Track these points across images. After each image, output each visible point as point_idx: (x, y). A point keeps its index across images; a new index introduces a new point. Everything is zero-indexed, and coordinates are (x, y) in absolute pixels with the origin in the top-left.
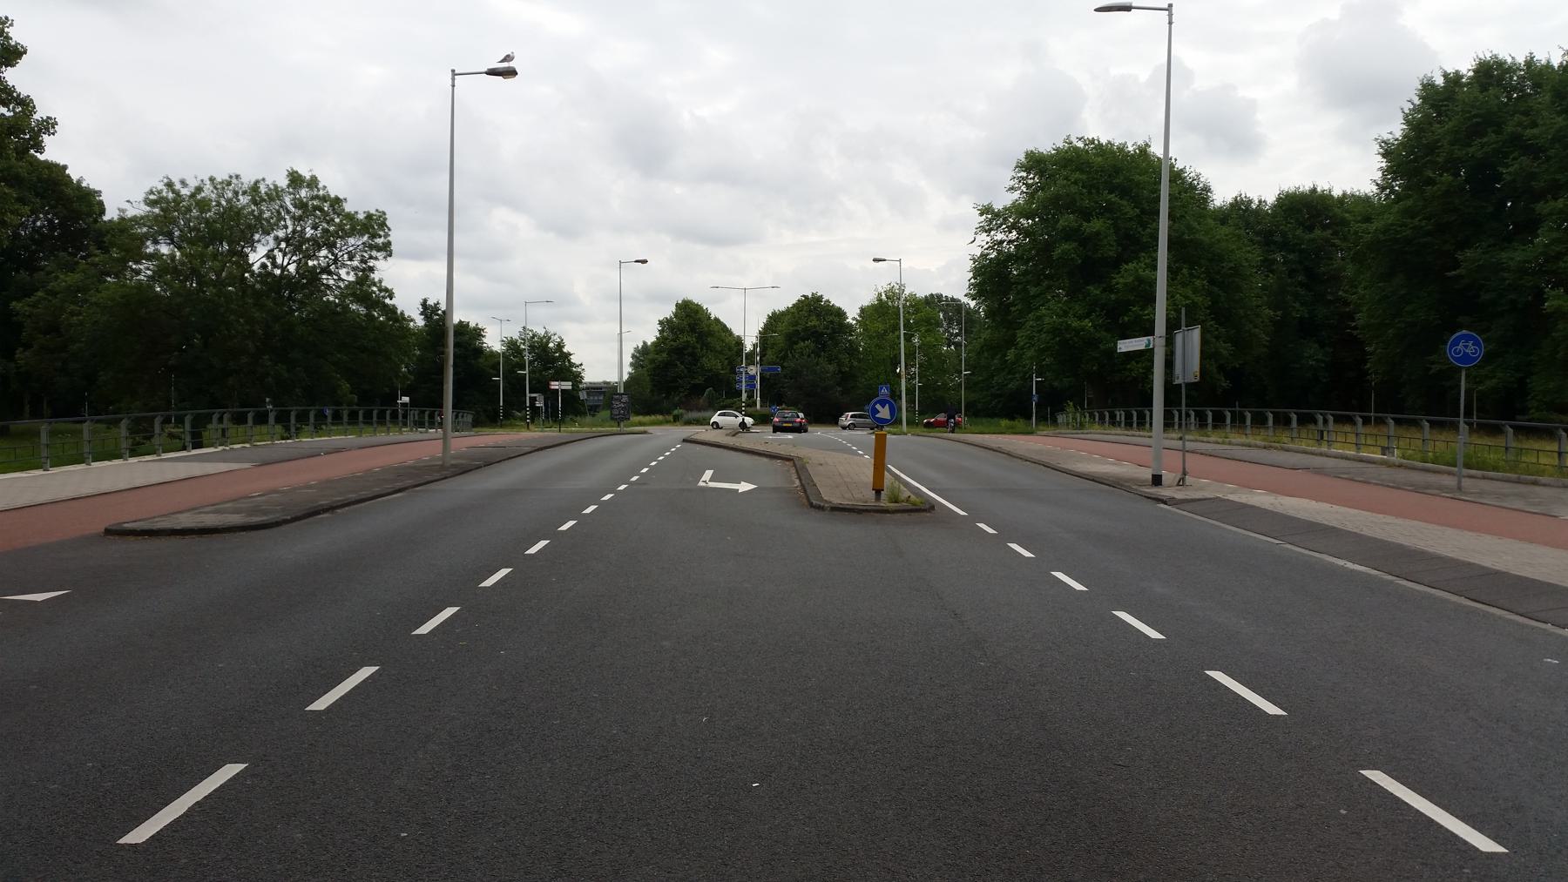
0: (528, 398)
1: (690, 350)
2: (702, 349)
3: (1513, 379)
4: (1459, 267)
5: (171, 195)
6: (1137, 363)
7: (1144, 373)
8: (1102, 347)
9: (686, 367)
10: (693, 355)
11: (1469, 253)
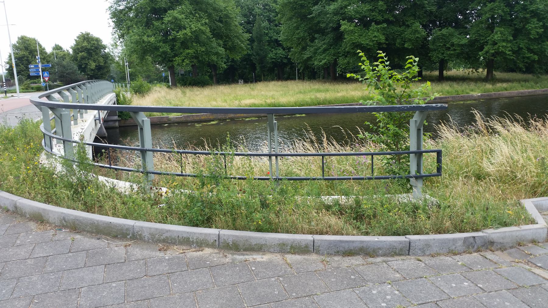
1: (26, 58)
2: (32, 57)
4: (312, 14)
5: (406, 67)
8: (161, 50)
9: (25, 66)
10: (27, 60)
11: (316, 7)
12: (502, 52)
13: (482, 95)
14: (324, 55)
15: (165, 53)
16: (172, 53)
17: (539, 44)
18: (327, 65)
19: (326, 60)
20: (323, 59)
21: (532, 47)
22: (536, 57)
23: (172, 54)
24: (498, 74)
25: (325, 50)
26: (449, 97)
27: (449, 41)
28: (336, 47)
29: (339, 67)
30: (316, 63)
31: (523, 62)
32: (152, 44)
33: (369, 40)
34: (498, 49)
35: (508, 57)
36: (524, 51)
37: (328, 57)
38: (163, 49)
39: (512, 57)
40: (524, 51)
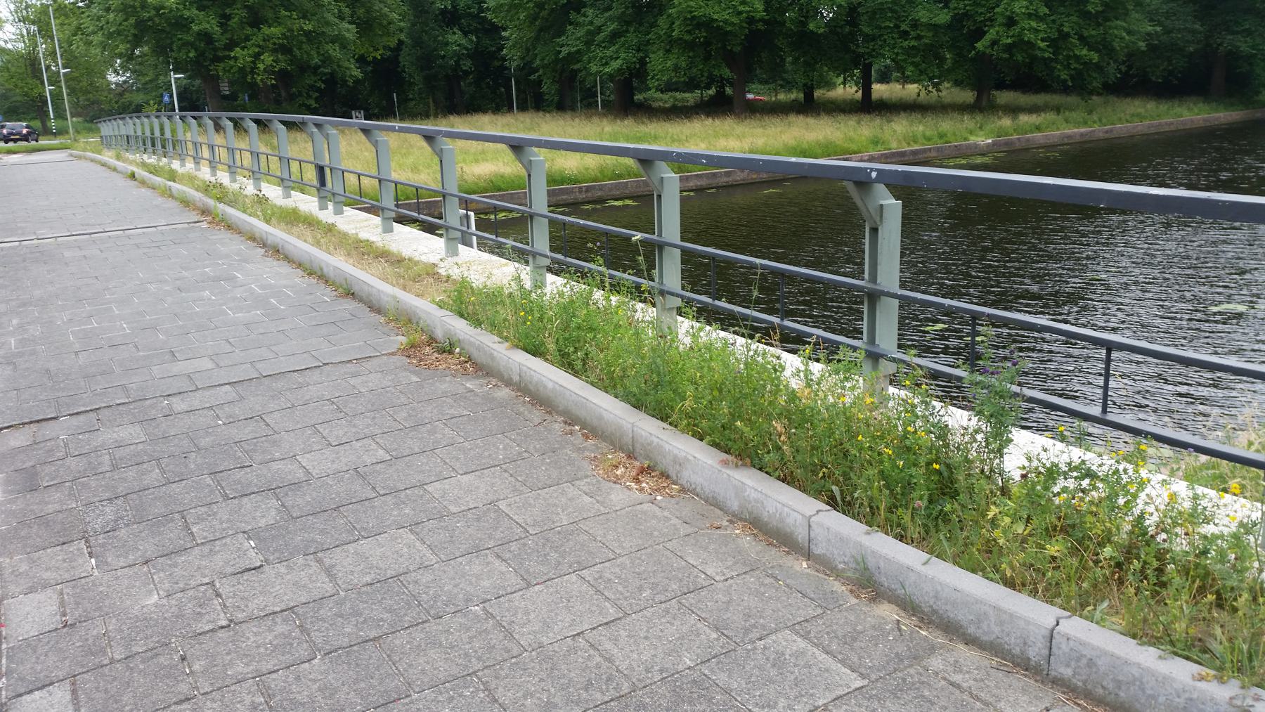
0: (173, 80)
3: (634, 59)
6: (243, 48)
7: (251, 62)
8: (195, 28)
12: (1029, 42)
13: (994, 143)
14: (613, 48)
15: (206, 37)
16: (223, 38)
17: (1099, 25)
18: (623, 73)
19: (619, 62)
20: (611, 58)
21: (1086, 34)
22: (1095, 57)
23: (224, 40)
24: (1004, 97)
25: (615, 36)
26: (930, 149)
27: (907, 17)
28: (641, 29)
29: (652, 79)
30: (594, 68)
31: (1068, 66)
32: (171, 11)
33: (731, 11)
34: (1020, 34)
35: (1039, 53)
36: (1071, 42)
37: (625, 52)
38: (201, 27)
39: (1046, 55)
40: (1074, 41)
